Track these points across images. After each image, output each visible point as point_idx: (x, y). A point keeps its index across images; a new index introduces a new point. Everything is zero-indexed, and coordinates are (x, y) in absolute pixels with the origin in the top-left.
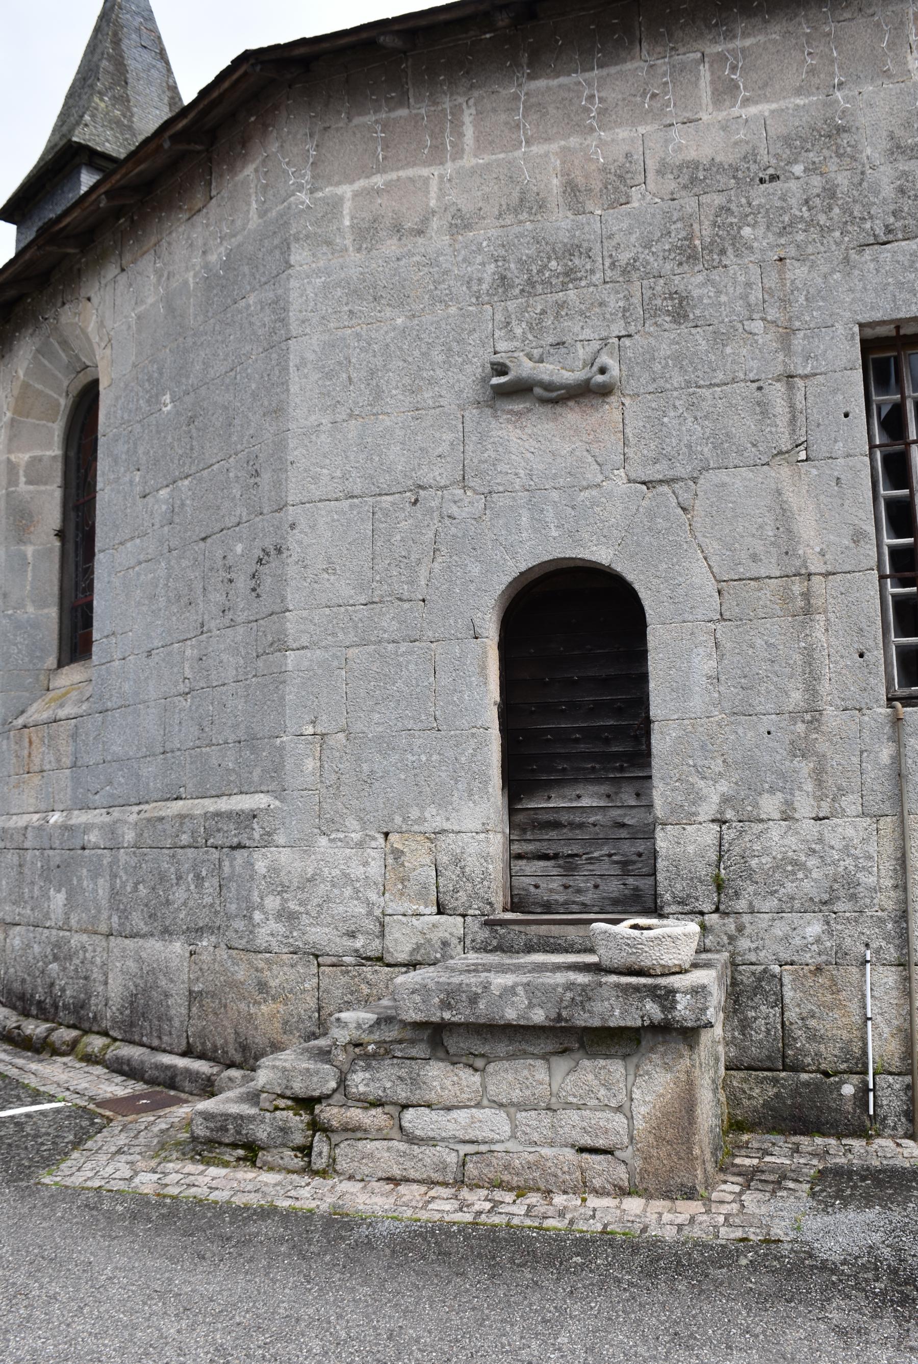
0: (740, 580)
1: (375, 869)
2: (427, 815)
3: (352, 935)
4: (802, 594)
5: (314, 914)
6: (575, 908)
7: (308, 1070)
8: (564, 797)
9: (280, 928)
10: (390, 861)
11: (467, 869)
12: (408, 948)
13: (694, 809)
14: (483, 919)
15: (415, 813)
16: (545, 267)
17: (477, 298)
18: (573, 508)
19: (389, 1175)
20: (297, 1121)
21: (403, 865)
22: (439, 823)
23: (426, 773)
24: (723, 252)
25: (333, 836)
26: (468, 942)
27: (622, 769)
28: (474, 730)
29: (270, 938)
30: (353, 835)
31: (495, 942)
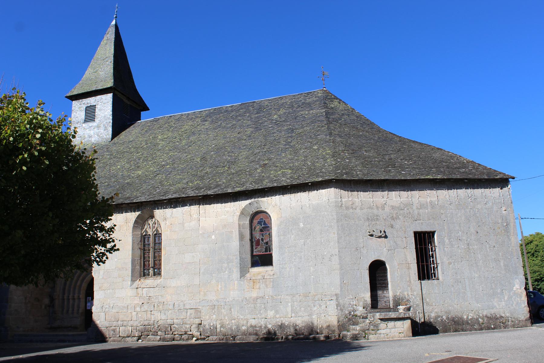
15: (360, 294)
16: (374, 217)
24: (397, 219)
27: (384, 288)
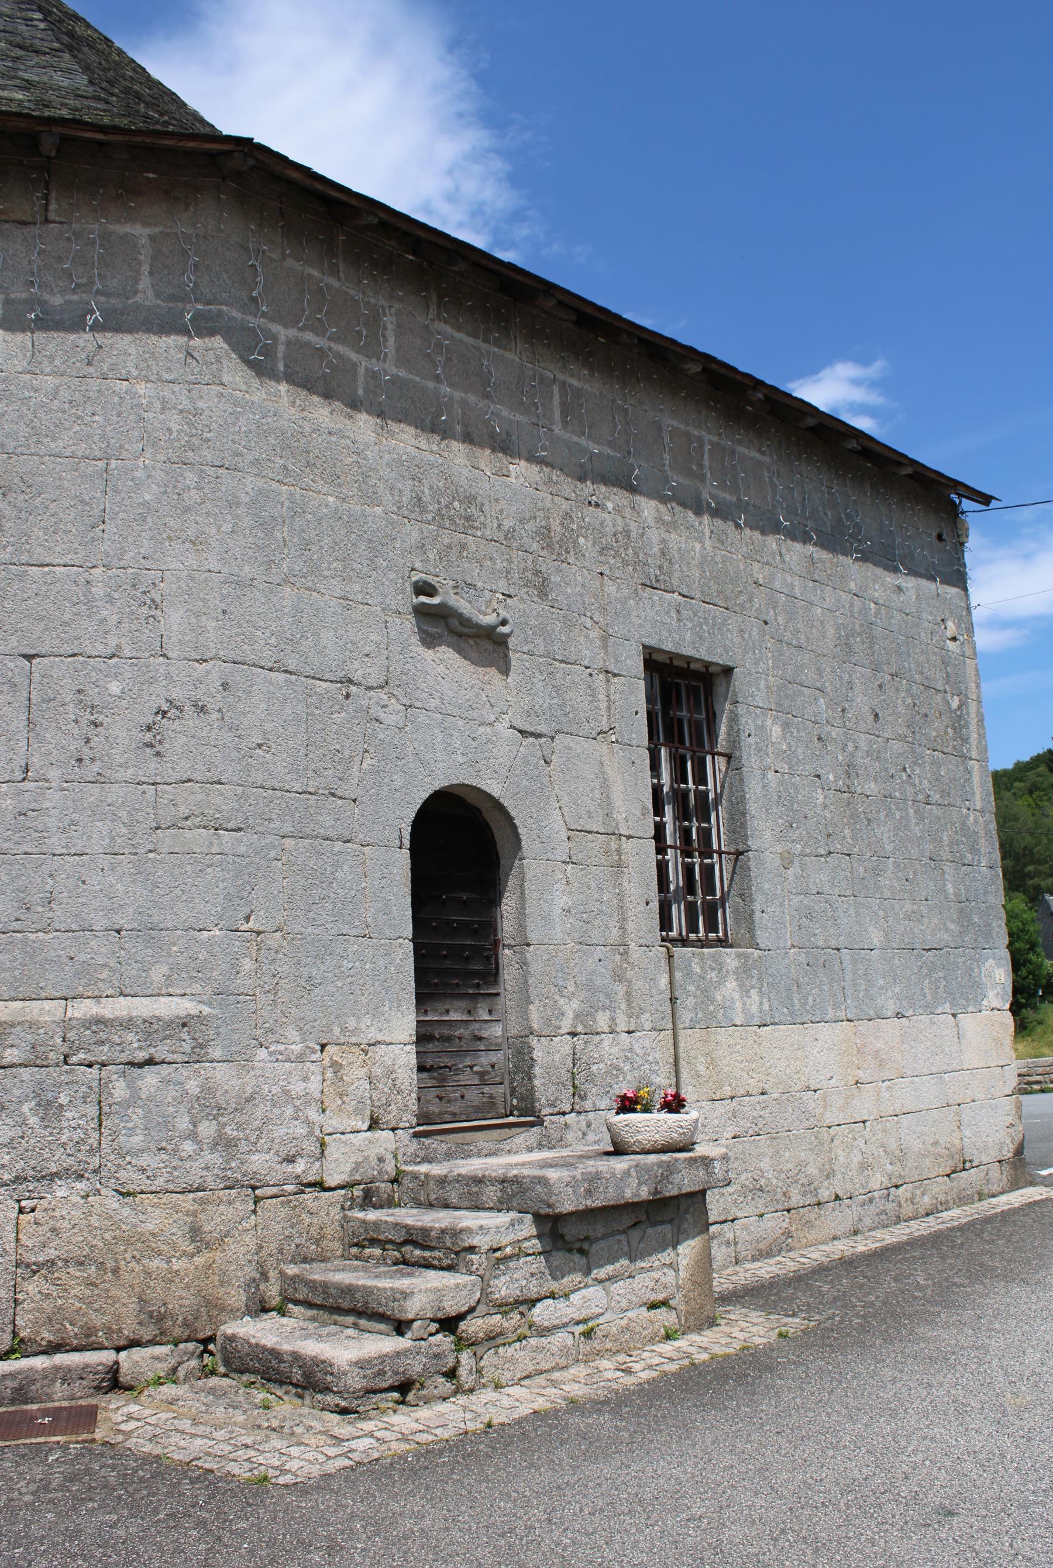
0: (581, 831)
1: (314, 1086)
2: (363, 1026)
3: (290, 1160)
4: (616, 850)
5: (253, 1139)
6: (448, 1117)
7: (457, 1285)
8: (435, 1011)
9: (215, 1159)
10: (329, 1074)
11: (398, 1082)
12: (347, 1168)
13: (558, 1023)
14: (412, 1131)
15: (352, 1023)
17: (399, 508)
18: (474, 739)
19: (527, 1373)
20: (443, 1341)
21: (342, 1079)
22: (373, 1035)
23: (361, 982)
25: (272, 1049)
26: (400, 1157)
28: (401, 940)
29: (205, 1173)
30: (293, 1047)
31: (422, 1154)
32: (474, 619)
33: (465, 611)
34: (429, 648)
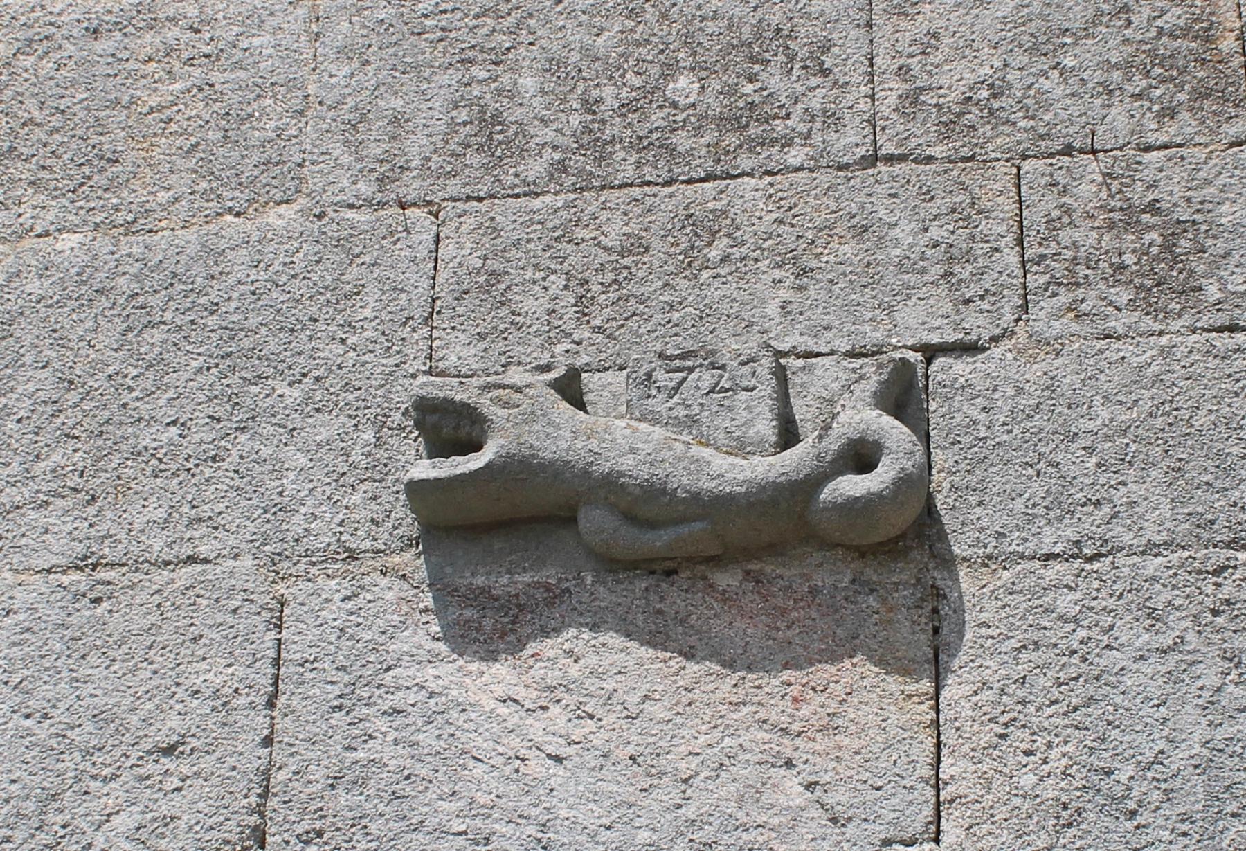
32: (682, 480)
33: (627, 464)
34: (492, 656)
